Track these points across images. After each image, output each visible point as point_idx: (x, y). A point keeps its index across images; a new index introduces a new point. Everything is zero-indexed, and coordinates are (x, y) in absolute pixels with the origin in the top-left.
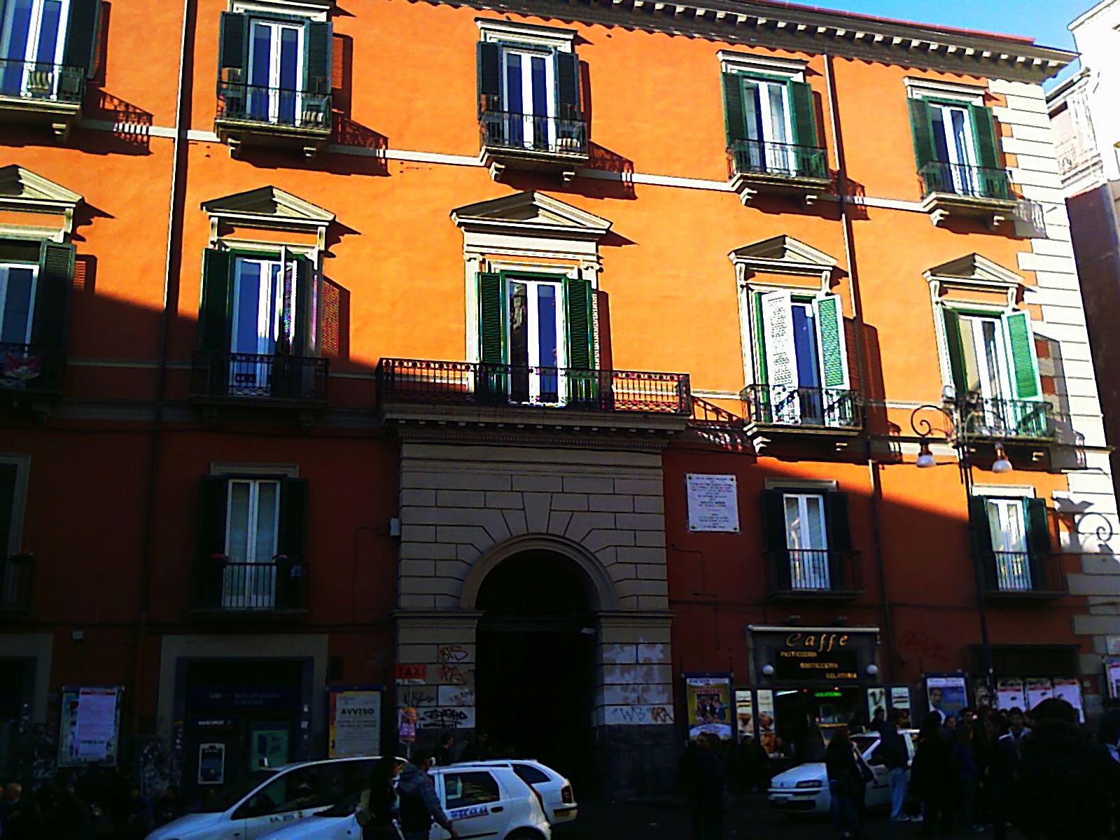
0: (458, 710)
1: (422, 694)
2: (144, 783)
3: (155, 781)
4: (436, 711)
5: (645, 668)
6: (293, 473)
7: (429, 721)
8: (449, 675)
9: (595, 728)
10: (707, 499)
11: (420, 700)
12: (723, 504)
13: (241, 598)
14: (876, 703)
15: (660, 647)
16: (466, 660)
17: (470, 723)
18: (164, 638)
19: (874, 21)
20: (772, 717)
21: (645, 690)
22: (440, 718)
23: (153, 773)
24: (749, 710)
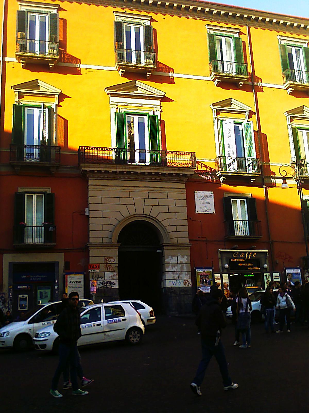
0: (112, 281)
4: (104, 282)
5: (180, 265)
6: (49, 191)
7: (101, 285)
8: (108, 268)
9: (163, 288)
10: (203, 201)
11: (98, 278)
12: (208, 203)
13: (31, 239)
14: (267, 279)
15: (186, 257)
18: (4, 255)
19: (272, 14)
20: (228, 284)
21: (181, 274)
22: (105, 285)
24: (219, 282)
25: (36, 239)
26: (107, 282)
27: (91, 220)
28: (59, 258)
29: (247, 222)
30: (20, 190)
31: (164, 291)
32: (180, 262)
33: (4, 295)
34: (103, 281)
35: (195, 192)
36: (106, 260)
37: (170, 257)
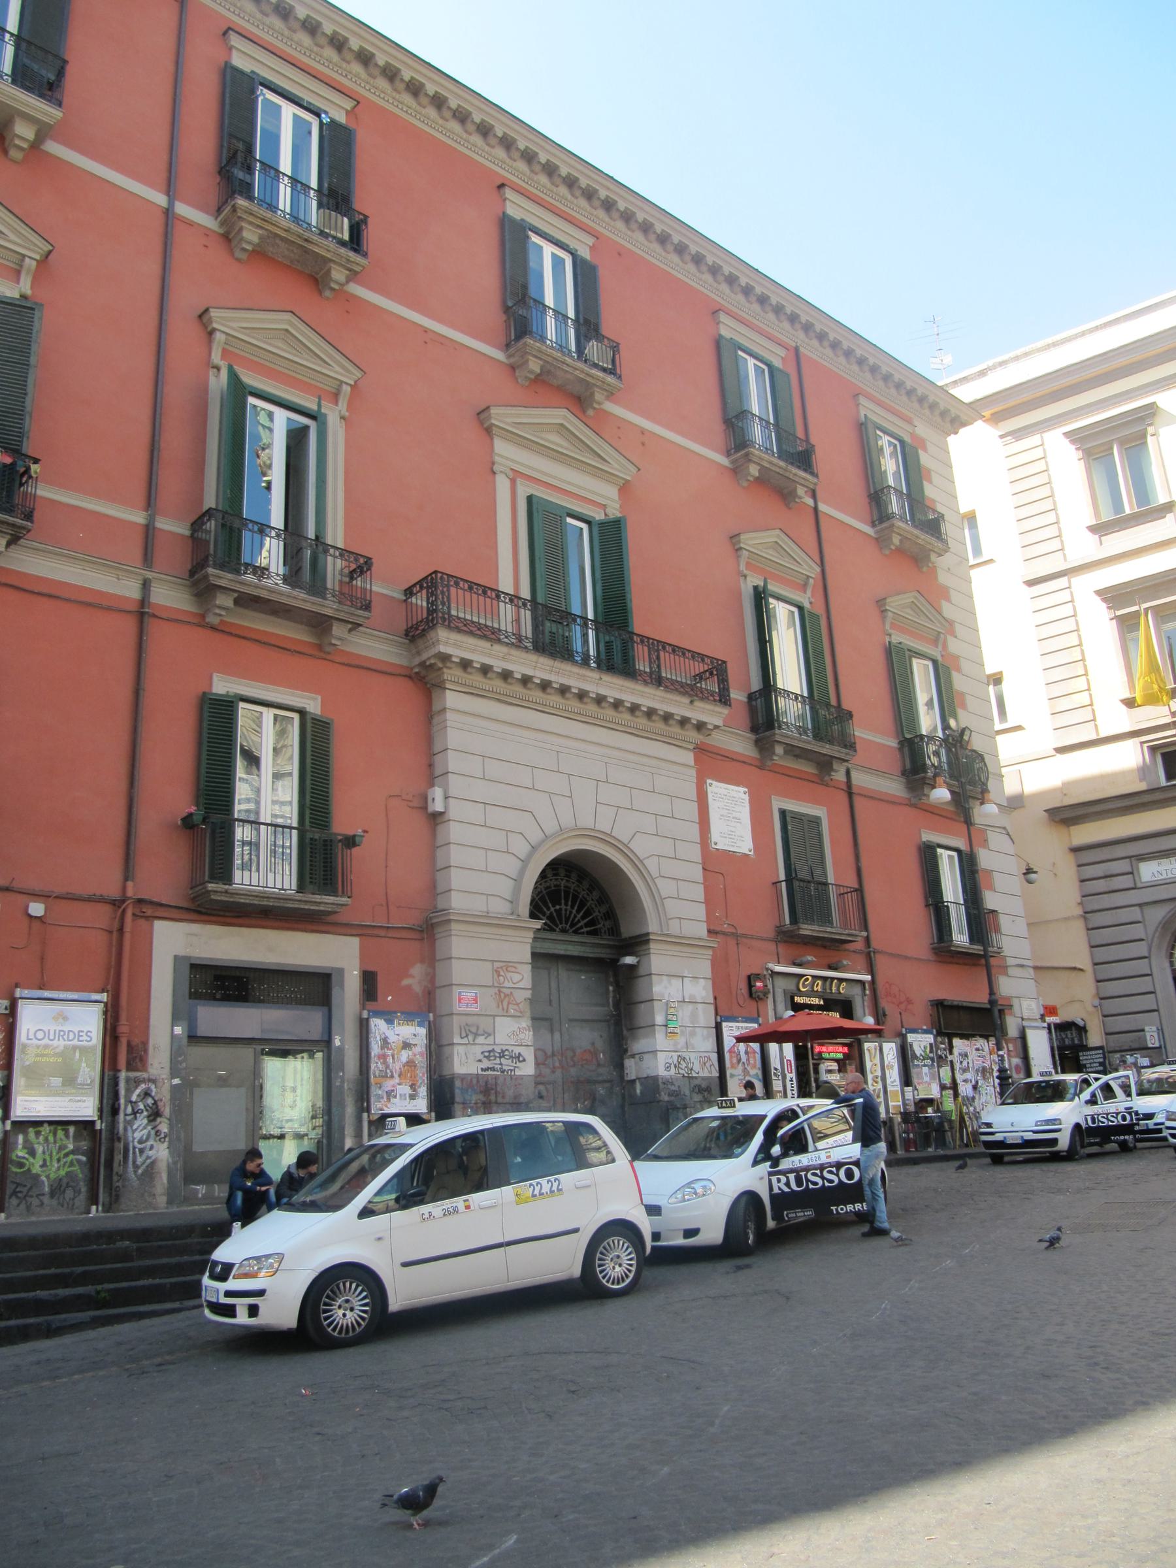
0: (517, 1050)
1: (478, 1028)
2: (134, 1148)
3: (149, 1143)
4: (493, 1050)
5: (691, 1006)
6: (313, 706)
7: (486, 1064)
8: (505, 1003)
9: (633, 1081)
10: (725, 812)
11: (476, 1035)
13: (255, 875)
16: (521, 985)
17: (528, 1069)
18: (158, 924)
21: (693, 1034)
22: (498, 1061)
23: (145, 1132)
25: (271, 876)
26: (503, 1051)
27: (455, 832)
28: (335, 953)
29: (295, 832)
30: (222, 686)
31: (638, 1091)
32: (691, 996)
33: (153, 1087)
34: (490, 1048)
35: (709, 781)
36: (499, 975)
37: (664, 978)
